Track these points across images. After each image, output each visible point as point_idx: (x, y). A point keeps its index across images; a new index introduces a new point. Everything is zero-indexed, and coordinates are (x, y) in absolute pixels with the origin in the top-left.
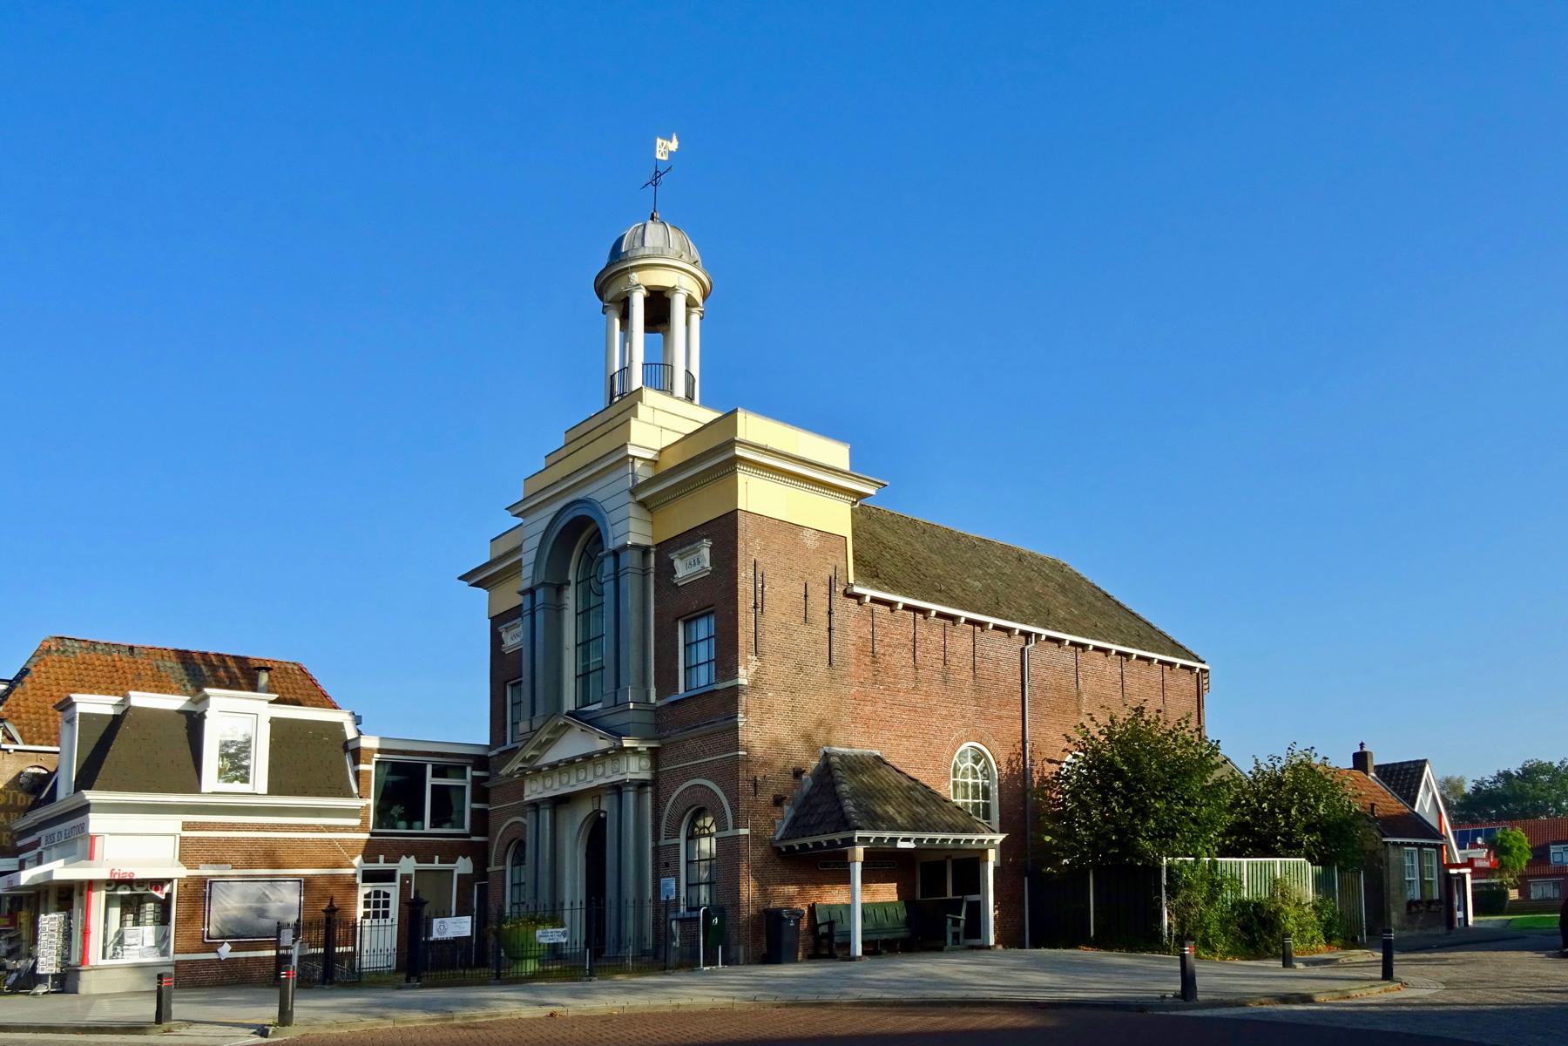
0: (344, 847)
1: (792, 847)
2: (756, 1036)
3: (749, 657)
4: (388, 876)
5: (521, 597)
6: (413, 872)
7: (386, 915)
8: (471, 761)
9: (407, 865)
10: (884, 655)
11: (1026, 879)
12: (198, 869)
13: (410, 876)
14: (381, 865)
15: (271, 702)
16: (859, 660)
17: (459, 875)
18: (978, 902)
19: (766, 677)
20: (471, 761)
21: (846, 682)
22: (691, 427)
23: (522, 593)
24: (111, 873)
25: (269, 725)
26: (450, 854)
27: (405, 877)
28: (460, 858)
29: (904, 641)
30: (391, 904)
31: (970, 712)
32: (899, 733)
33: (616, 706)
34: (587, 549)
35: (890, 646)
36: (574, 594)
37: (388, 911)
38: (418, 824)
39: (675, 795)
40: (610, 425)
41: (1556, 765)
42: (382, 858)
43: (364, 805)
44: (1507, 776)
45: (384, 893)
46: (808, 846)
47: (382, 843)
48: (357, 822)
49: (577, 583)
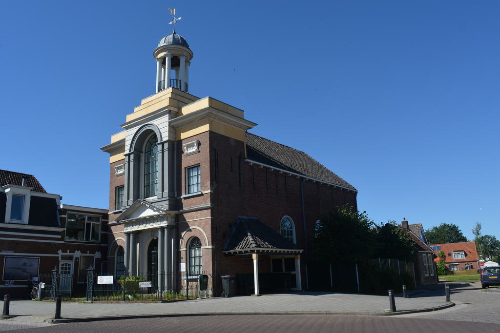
1: (231, 253)
2: (25, 326)
4: (71, 258)
7: (69, 273)
8: (101, 215)
11: (496, 277)
13: (78, 258)
14: (68, 254)
15: (31, 190)
17: (96, 259)
18: (295, 274)
22: (170, 95)
23: (126, 155)
27: (77, 258)
30: (71, 269)
33: (162, 198)
34: (150, 141)
40: (160, 99)
41: (450, 225)
42: (68, 251)
44: (436, 228)
48: (60, 237)
49: (145, 153)
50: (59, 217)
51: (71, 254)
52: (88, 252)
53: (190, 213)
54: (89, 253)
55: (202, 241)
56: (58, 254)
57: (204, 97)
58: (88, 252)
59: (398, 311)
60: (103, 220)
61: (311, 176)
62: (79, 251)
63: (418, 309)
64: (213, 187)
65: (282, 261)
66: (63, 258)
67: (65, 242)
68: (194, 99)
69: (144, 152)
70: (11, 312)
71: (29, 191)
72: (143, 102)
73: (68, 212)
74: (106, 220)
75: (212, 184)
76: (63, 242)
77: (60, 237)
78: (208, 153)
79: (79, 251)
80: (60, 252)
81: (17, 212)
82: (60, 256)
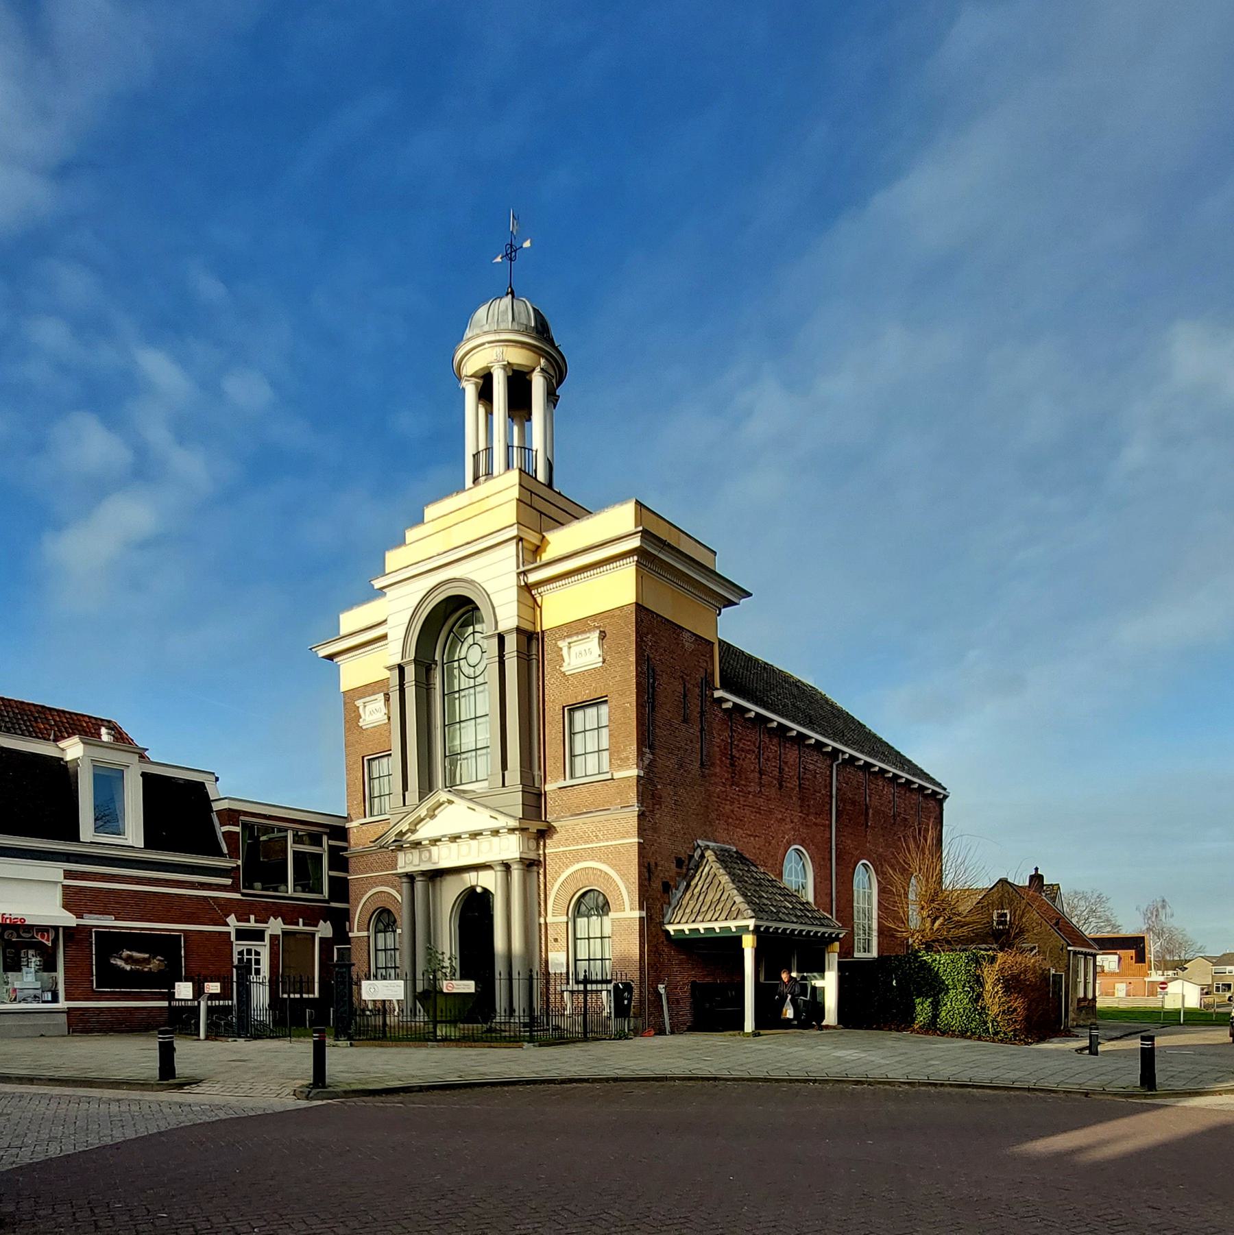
0: (219, 906)
3: (644, 749)
4: (258, 935)
5: (388, 672)
6: (280, 933)
8: (328, 831)
9: (275, 926)
10: (739, 759)
12: (82, 918)
14: (252, 924)
16: (722, 761)
17: (321, 939)
19: (655, 770)
20: (328, 831)
21: (712, 782)
23: (390, 668)
24: (3, 918)
25: (141, 778)
26: (313, 917)
27: (274, 938)
28: (321, 921)
29: (752, 747)
31: (797, 815)
32: (749, 833)
35: (743, 751)
36: (441, 674)
37: (259, 969)
38: (282, 888)
39: (563, 877)
42: (252, 917)
43: (235, 865)
45: (255, 951)
46: (731, 929)
47: (251, 904)
48: (228, 881)
49: (443, 664)
50: (221, 830)
51: (261, 926)
52: (301, 920)
56: (227, 925)
57: (621, 500)
60: (332, 843)
64: (642, 760)
66: (242, 935)
67: (243, 895)
68: (575, 512)
69: (439, 663)
70: (182, 1067)
71: (397, 660)
72: (431, 512)
73: (242, 818)
75: (640, 754)
76: (238, 896)
77: (228, 881)
78: (633, 668)
80: (232, 920)
81: (108, 818)
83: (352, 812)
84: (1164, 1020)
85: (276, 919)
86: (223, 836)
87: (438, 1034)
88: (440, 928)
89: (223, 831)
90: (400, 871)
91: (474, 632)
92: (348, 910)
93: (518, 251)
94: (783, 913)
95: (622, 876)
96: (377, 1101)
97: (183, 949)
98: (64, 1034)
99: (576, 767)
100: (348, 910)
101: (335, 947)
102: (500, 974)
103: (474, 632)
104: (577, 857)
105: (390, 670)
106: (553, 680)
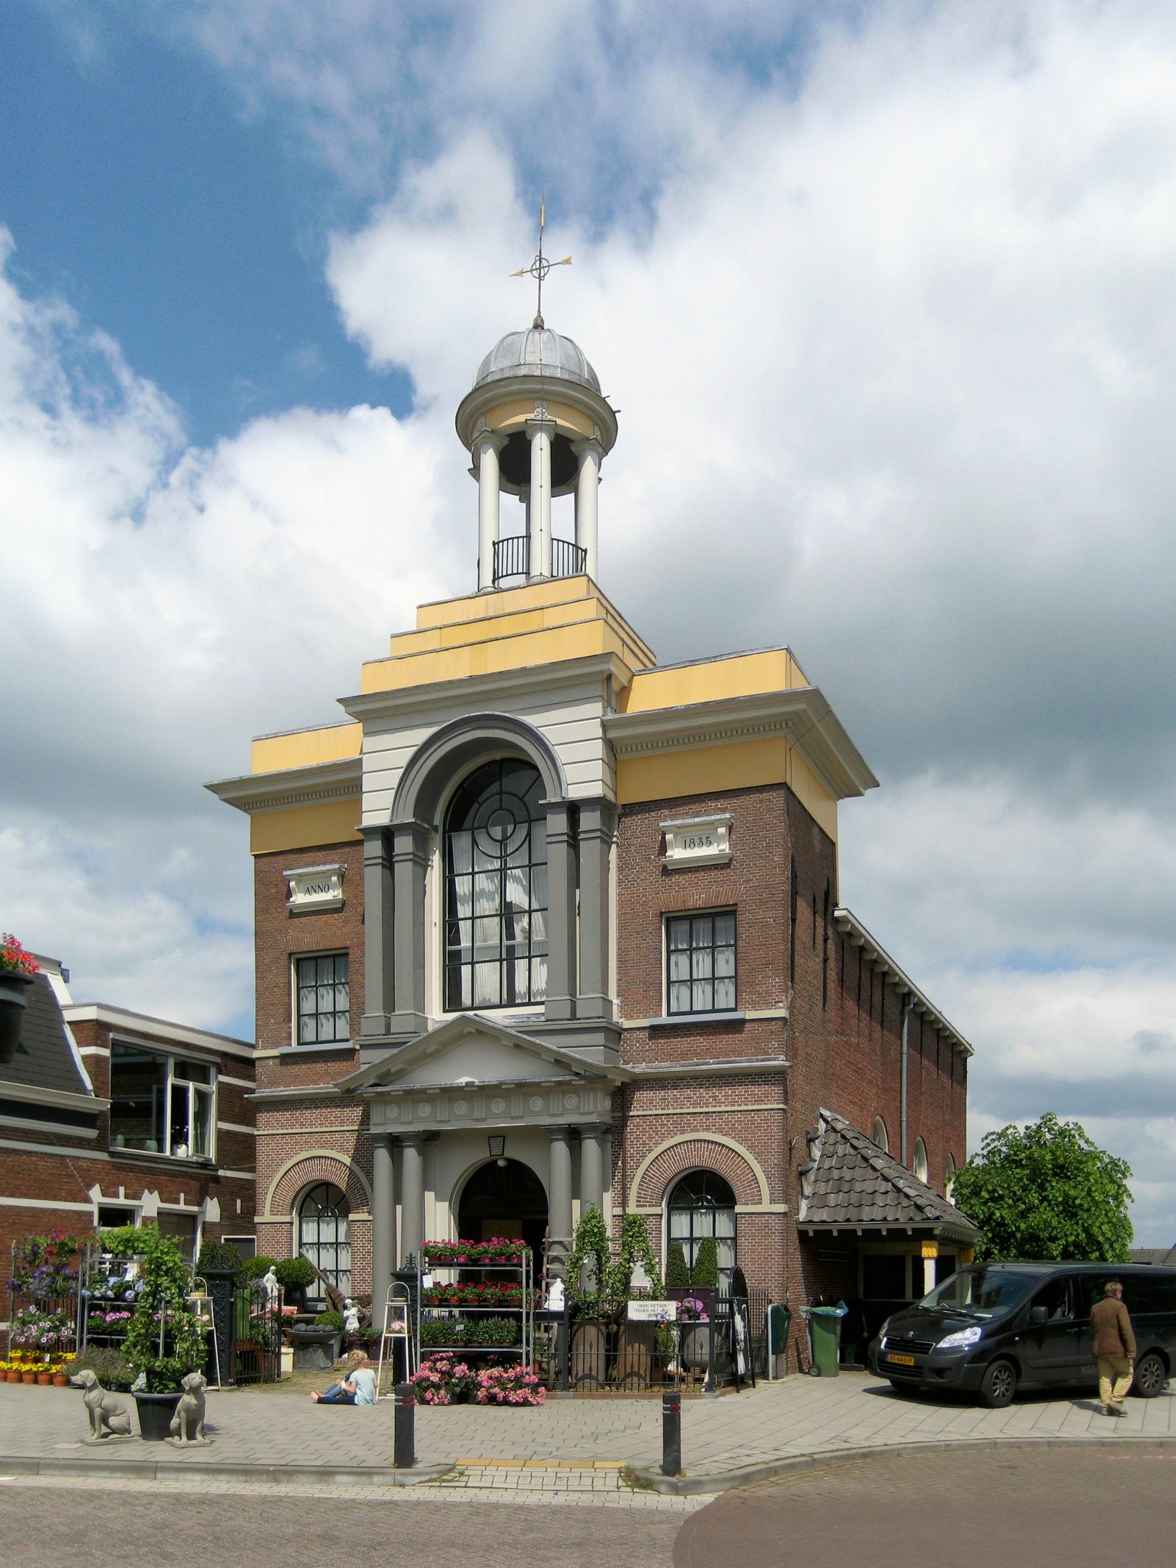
42: (122, 1190)
50: (79, 1053)
52: (182, 1195)
53: (520, 843)
54: (127, 1197)
55: (724, 1168)
56: (88, 1200)
58: (182, 1195)
59: (394, 1034)
61: (197, 1102)
62: (156, 1193)
63: (567, 601)
65: (248, 1125)
74: (771, 1377)
76: (104, 1156)
77: (92, 1133)
79: (156, 1193)
80: (95, 1193)
82: (94, 1209)
83: (545, 335)
84: (535, 1338)
85: (151, 1193)
86: (768, 1375)
87: (721, 1265)
88: (475, 1165)
89: (82, 1053)
90: (374, 1130)
91: (500, 793)
92: (252, 1183)
93: (530, 269)
94: (624, 1204)
95: (758, 1155)
96: (382, 729)
97: (865, 1325)
98: (372, 1460)
99: (440, 983)
100: (252, 1183)
101: (223, 1237)
102: (727, 993)
103: (500, 793)
104: (680, 1122)
105: (360, 716)
106: (644, 874)
